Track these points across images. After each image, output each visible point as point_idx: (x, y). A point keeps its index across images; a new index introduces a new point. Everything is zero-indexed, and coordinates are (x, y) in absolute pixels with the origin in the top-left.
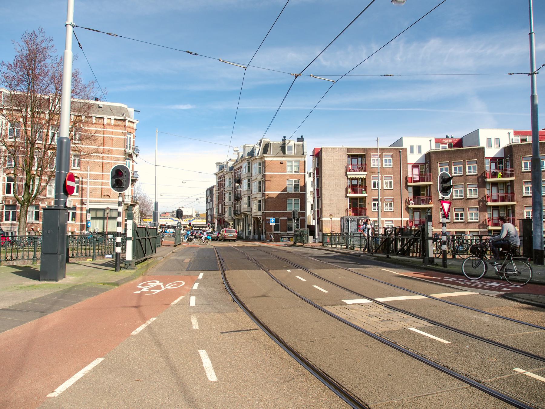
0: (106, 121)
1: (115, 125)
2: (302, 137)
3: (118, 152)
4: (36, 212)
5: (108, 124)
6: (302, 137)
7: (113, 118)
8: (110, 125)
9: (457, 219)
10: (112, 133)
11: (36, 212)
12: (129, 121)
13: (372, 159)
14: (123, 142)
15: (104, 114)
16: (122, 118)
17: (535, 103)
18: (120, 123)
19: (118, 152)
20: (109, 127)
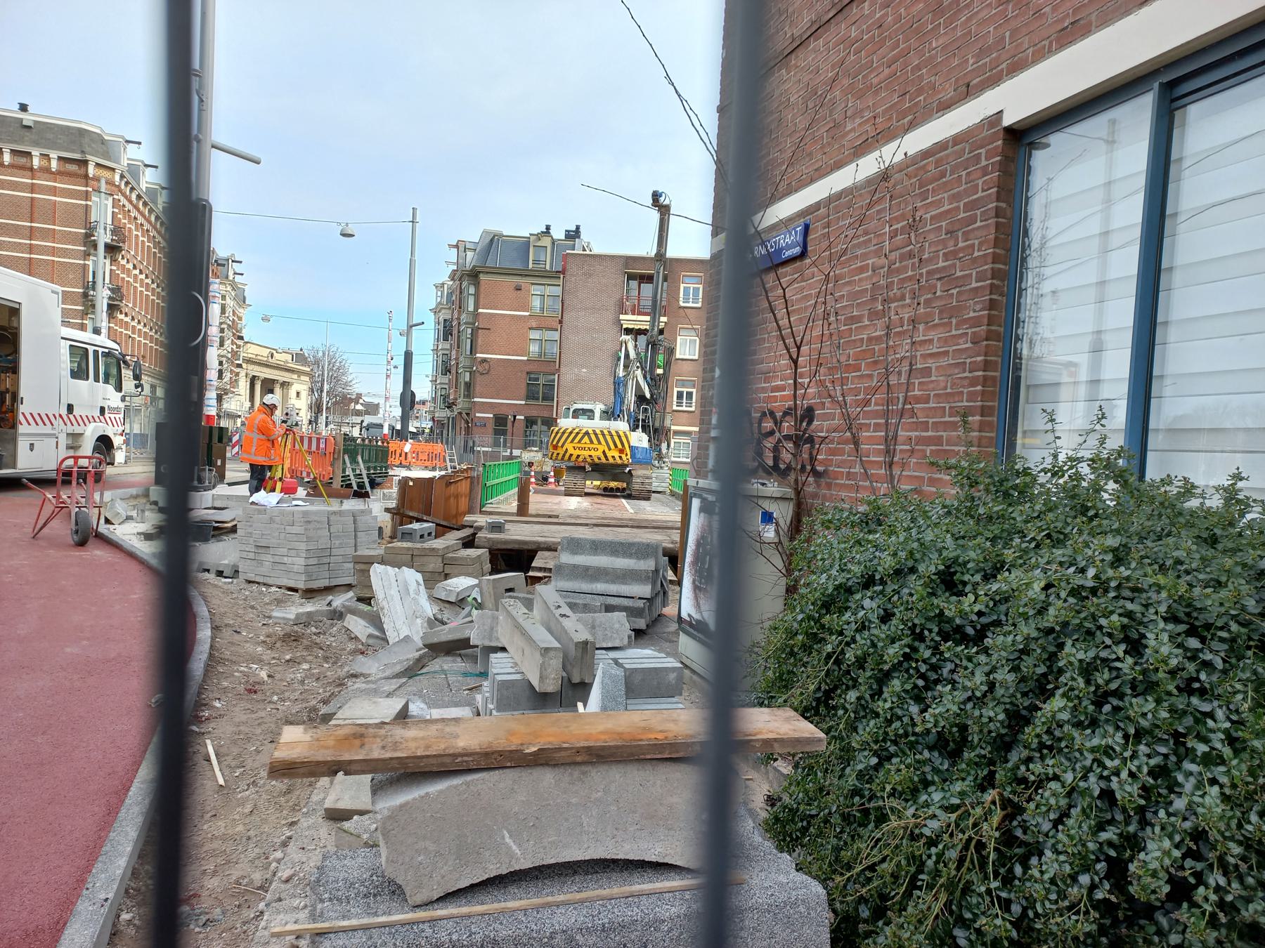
0: (36, 162)
1: (59, 173)
2: (578, 227)
3: (67, 238)
4: (601, 419)
5: (41, 169)
6: (578, 227)
7: (54, 155)
8: (46, 170)
9: (679, 404)
10: (54, 191)
11: (601, 419)
12: (98, 165)
13: (682, 286)
14: (36, 215)
15: (36, 144)
16: (77, 156)
17: (194, 197)
18: (73, 168)
19: (67, 238)
20: (46, 175)
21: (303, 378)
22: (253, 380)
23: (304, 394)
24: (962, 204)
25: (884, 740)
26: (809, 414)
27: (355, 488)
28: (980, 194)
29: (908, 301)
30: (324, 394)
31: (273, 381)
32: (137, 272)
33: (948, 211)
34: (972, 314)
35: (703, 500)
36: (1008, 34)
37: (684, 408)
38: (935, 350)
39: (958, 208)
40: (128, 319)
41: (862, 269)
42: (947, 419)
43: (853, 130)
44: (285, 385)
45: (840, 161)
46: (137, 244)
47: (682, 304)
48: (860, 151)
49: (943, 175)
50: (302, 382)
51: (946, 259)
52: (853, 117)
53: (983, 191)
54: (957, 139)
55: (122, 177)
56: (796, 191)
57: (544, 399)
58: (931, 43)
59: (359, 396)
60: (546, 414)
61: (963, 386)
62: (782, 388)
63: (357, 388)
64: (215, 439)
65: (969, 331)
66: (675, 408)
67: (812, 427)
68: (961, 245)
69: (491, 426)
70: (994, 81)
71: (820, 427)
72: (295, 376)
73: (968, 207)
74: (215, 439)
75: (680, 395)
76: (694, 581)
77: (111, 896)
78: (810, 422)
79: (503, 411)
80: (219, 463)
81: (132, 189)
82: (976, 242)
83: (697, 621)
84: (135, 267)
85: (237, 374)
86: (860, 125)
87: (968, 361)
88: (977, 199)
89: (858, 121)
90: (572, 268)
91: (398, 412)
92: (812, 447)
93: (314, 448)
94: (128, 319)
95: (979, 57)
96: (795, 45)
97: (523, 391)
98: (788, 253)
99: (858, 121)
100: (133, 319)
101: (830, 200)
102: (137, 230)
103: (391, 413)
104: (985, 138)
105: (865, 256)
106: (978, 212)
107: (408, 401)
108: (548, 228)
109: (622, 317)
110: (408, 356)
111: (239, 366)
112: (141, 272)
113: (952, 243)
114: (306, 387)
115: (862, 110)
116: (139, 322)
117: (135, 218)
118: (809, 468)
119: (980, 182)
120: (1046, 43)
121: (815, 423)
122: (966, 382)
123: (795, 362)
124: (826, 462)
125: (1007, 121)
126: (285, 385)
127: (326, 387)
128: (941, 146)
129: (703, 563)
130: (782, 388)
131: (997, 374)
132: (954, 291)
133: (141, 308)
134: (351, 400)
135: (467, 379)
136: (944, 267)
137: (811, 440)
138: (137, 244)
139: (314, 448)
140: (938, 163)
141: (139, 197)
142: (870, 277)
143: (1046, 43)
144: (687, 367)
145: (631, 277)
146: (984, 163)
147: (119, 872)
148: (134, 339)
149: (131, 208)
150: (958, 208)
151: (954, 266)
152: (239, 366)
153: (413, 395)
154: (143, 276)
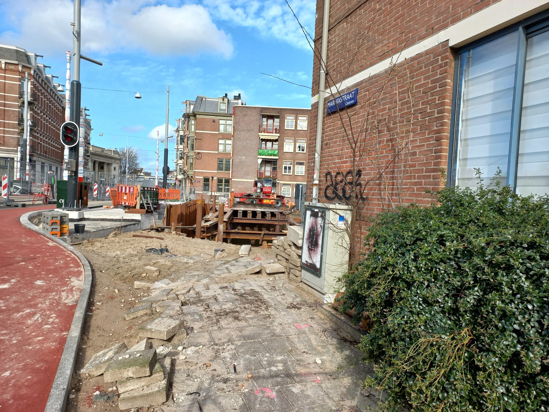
2: (240, 95)
6: (240, 95)
9: (285, 172)
21: (117, 161)
22: (94, 162)
23: (117, 168)
24: (430, 80)
25: (455, 311)
26: (359, 173)
27: (146, 209)
28: (439, 76)
29: (405, 123)
30: (127, 169)
31: (103, 163)
32: (42, 114)
33: (424, 84)
34: (435, 128)
35: (312, 211)
36: (451, 6)
37: (287, 174)
38: (418, 144)
39: (428, 82)
40: (36, 134)
41: (384, 109)
42: (424, 174)
43: (378, 49)
44: (109, 164)
45: (373, 62)
46: (42, 102)
47: (286, 128)
48: (382, 57)
49: (421, 68)
50: (117, 163)
51: (423, 104)
52: (378, 44)
53: (440, 74)
54: (427, 53)
55: (35, 71)
56: (352, 76)
57: (225, 170)
58: (415, 11)
59: (142, 169)
60: (226, 177)
61: (432, 160)
62: (346, 162)
63: (141, 166)
64: (83, 188)
65: (434, 136)
66: (283, 173)
67: (360, 179)
68: (430, 98)
69: (202, 182)
70: (444, 27)
71: (364, 178)
72: (113, 161)
73: (433, 82)
74: (83, 188)
75: (285, 168)
76: (308, 247)
77: (65, 387)
78: (360, 176)
79: (208, 176)
80: (85, 198)
81: (39, 77)
82: (437, 97)
83: (311, 264)
84: (41, 112)
85: (88, 160)
86: (381, 47)
87: (434, 148)
88: (438, 78)
89: (381, 45)
90: (238, 112)
91: (162, 175)
92: (361, 187)
93: (127, 191)
94: (38, 135)
95: (437, 16)
96: (350, 12)
97: (216, 166)
98: (349, 103)
99: (381, 45)
100: (41, 135)
101: (370, 78)
102: (42, 95)
103: (158, 175)
104: (440, 52)
105: (384, 104)
106: (438, 84)
107: (166, 171)
108: (226, 95)
109: (260, 134)
110: (166, 151)
111: (89, 156)
112: (44, 114)
113: (426, 97)
114: (118, 165)
115: (382, 41)
116: (44, 137)
117: (41, 90)
118: (359, 196)
119: (439, 71)
120: (469, 10)
121: (362, 177)
122: (433, 158)
123: (354, 150)
124: (368, 194)
125: (451, 44)
126: (109, 164)
127: (127, 166)
128: (419, 56)
129: (313, 238)
130: (346, 162)
131: (447, 154)
132: (427, 118)
133: (44, 130)
134: (139, 171)
135: (191, 162)
136: (422, 108)
137: (360, 184)
138: (42, 102)
139: (127, 191)
140: (418, 64)
141: (42, 80)
142: (388, 113)
143: (469, 10)
144: (288, 156)
145: (263, 116)
146: (440, 62)
147: (67, 377)
148: (41, 144)
149: (39, 85)
150: (428, 82)
151: (427, 107)
152: (89, 156)
153: (168, 168)
154: (45, 116)
